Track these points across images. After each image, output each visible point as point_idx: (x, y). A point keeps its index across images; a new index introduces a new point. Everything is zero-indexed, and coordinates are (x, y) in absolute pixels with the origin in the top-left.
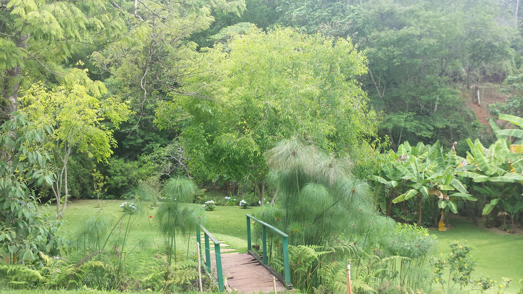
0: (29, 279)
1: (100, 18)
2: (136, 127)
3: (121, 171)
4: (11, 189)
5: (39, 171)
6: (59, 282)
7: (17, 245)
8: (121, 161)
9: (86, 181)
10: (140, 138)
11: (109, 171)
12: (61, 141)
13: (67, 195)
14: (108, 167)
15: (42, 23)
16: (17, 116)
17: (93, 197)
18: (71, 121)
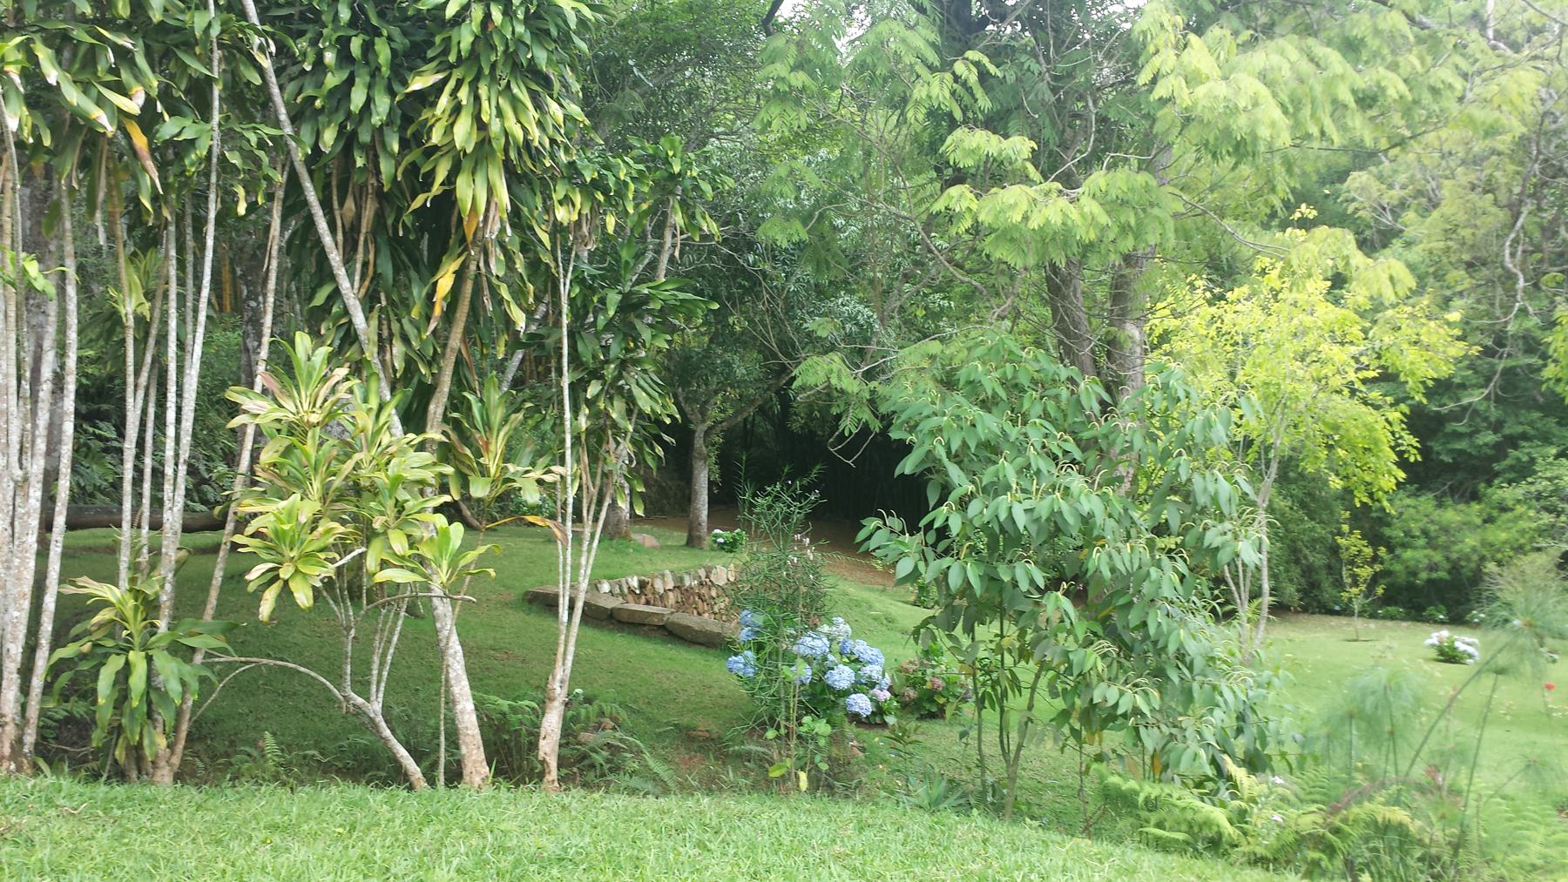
0: (1196, 829)
1: (1394, 67)
2: (1474, 398)
3: (1425, 533)
4: (1148, 574)
5: (1220, 527)
6: (1278, 851)
7: (1164, 728)
8: (1426, 502)
9: (1317, 559)
10: (1488, 428)
11: (1387, 531)
12: (1249, 443)
13: (1267, 600)
14: (1384, 520)
15: (1232, 111)
16: (1164, 375)
17: (1337, 608)
18: (1278, 384)
